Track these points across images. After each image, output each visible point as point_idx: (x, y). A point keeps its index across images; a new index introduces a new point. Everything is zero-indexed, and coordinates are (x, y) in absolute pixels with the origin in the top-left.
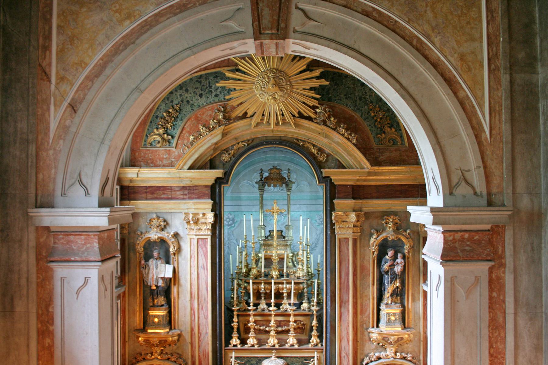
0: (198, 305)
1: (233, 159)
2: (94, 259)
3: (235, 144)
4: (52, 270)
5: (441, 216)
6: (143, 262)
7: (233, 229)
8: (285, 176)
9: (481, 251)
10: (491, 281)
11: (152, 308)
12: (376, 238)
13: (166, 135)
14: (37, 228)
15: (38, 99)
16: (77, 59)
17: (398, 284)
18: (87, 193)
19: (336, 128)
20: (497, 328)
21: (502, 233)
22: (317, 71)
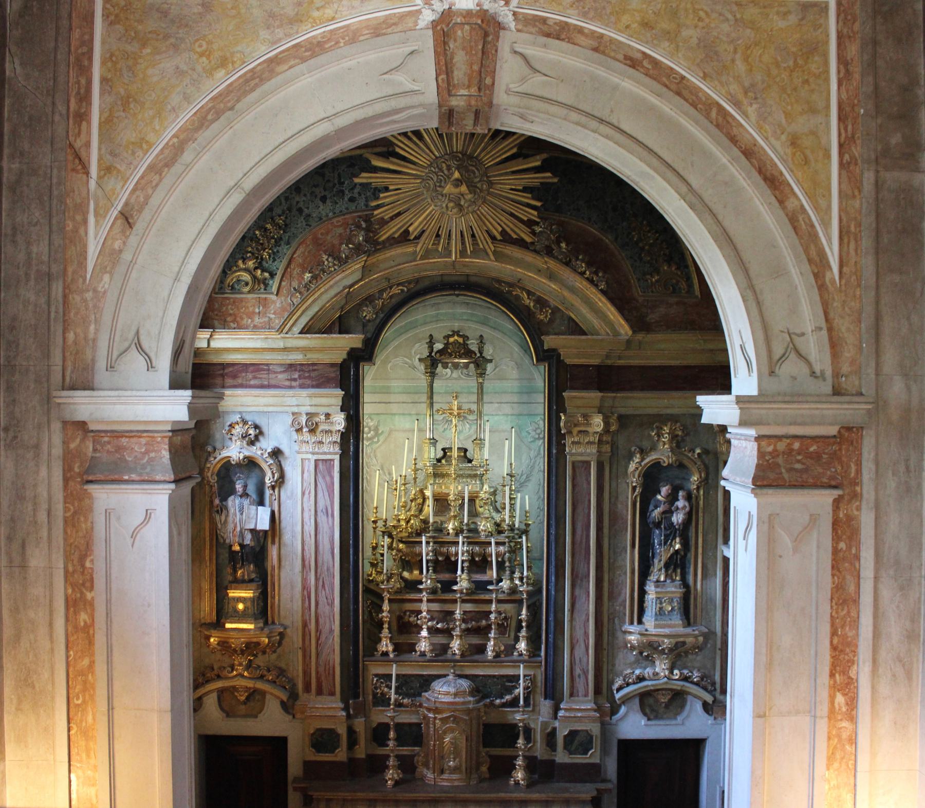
0: (317, 579)
1: (382, 316)
2: (163, 479)
3: (386, 289)
4: (90, 497)
5: (754, 411)
6: (217, 501)
7: (375, 446)
8: (474, 348)
9: (821, 470)
10: (836, 523)
11: (233, 585)
12: (640, 463)
13: (259, 272)
14: (65, 423)
15: (66, 204)
16: (134, 135)
17: (677, 547)
18: (150, 366)
19: (570, 260)
20: (845, 602)
21: (857, 442)
22: (538, 157)
